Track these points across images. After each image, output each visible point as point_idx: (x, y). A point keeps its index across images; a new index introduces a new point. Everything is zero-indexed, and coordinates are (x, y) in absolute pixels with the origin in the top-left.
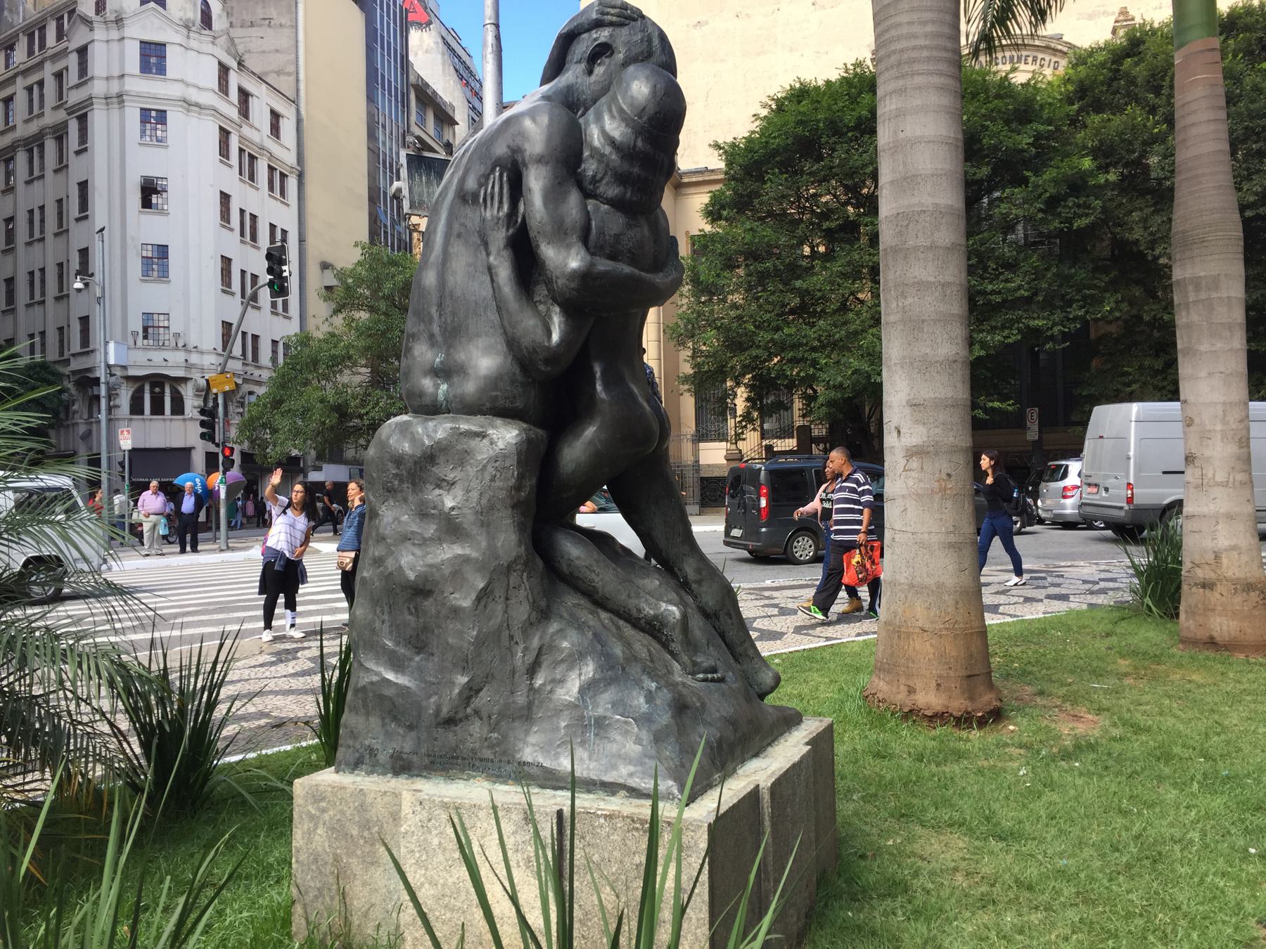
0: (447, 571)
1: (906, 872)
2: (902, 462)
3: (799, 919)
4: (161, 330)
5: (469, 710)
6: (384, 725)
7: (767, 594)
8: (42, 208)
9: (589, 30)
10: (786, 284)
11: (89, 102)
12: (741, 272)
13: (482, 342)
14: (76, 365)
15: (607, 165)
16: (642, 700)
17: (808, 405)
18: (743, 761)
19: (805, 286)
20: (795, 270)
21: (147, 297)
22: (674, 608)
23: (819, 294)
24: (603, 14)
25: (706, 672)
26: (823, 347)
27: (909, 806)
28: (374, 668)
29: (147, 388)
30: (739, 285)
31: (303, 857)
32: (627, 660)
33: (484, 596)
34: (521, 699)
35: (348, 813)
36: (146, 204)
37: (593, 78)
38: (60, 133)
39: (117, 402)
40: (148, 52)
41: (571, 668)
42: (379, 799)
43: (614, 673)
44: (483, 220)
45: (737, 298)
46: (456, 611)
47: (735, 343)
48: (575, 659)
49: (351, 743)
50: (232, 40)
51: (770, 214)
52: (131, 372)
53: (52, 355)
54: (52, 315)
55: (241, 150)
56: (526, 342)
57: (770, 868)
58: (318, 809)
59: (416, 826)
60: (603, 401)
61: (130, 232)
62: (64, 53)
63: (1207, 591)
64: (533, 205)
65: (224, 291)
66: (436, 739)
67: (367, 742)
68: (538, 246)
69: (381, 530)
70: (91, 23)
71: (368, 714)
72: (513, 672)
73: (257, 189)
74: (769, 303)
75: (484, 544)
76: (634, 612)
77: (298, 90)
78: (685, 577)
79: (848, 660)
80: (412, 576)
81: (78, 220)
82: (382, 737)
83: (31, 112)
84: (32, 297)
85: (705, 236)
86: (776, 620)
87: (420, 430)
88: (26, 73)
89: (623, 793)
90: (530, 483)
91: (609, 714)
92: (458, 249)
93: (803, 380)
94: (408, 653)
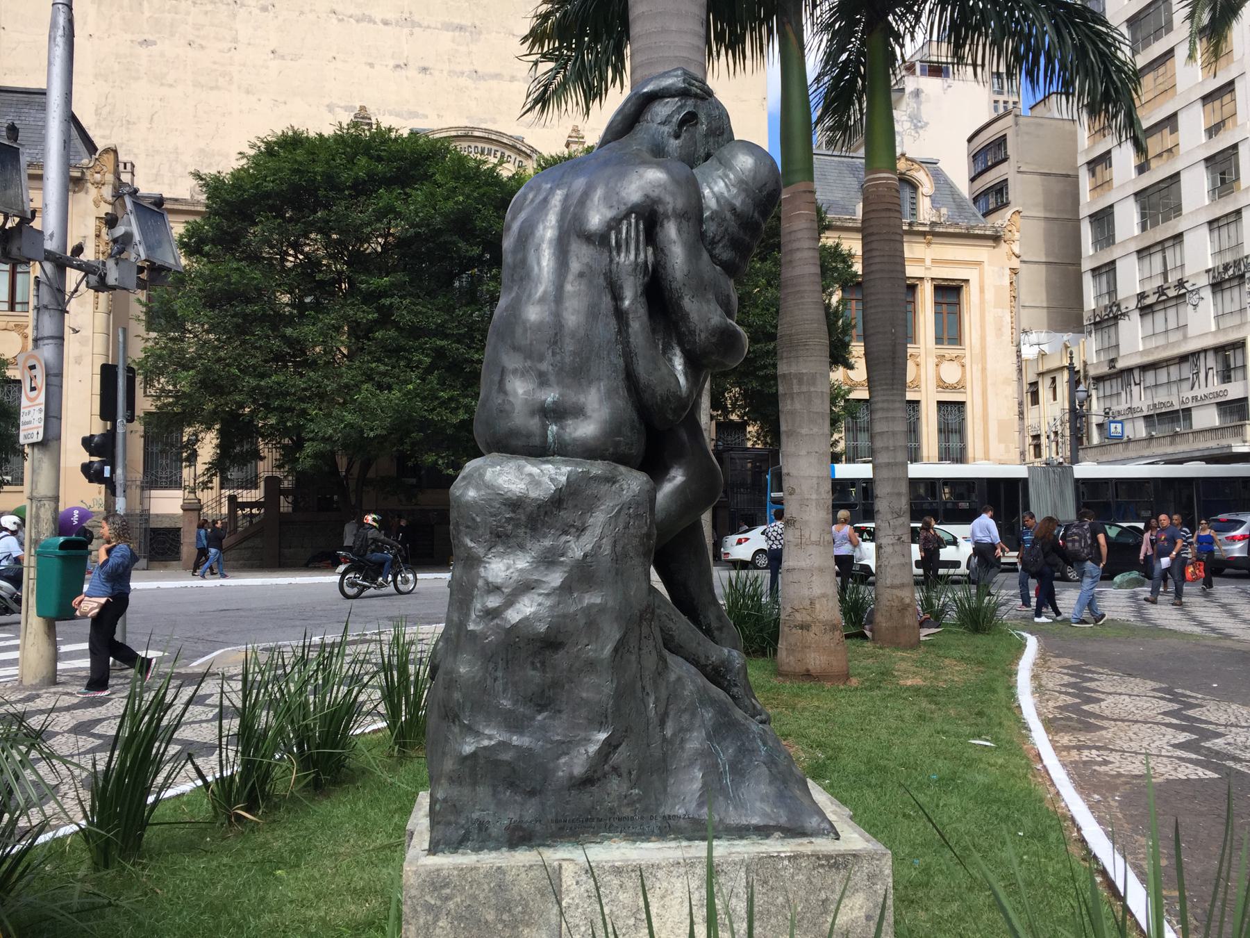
19: (295, 335)
42: (523, 875)
47: (210, 385)
49: (452, 818)
59: (581, 897)
66: (568, 803)
67: (475, 816)
72: (648, 724)
82: (492, 807)
89: (777, 834)
94: (528, 712)
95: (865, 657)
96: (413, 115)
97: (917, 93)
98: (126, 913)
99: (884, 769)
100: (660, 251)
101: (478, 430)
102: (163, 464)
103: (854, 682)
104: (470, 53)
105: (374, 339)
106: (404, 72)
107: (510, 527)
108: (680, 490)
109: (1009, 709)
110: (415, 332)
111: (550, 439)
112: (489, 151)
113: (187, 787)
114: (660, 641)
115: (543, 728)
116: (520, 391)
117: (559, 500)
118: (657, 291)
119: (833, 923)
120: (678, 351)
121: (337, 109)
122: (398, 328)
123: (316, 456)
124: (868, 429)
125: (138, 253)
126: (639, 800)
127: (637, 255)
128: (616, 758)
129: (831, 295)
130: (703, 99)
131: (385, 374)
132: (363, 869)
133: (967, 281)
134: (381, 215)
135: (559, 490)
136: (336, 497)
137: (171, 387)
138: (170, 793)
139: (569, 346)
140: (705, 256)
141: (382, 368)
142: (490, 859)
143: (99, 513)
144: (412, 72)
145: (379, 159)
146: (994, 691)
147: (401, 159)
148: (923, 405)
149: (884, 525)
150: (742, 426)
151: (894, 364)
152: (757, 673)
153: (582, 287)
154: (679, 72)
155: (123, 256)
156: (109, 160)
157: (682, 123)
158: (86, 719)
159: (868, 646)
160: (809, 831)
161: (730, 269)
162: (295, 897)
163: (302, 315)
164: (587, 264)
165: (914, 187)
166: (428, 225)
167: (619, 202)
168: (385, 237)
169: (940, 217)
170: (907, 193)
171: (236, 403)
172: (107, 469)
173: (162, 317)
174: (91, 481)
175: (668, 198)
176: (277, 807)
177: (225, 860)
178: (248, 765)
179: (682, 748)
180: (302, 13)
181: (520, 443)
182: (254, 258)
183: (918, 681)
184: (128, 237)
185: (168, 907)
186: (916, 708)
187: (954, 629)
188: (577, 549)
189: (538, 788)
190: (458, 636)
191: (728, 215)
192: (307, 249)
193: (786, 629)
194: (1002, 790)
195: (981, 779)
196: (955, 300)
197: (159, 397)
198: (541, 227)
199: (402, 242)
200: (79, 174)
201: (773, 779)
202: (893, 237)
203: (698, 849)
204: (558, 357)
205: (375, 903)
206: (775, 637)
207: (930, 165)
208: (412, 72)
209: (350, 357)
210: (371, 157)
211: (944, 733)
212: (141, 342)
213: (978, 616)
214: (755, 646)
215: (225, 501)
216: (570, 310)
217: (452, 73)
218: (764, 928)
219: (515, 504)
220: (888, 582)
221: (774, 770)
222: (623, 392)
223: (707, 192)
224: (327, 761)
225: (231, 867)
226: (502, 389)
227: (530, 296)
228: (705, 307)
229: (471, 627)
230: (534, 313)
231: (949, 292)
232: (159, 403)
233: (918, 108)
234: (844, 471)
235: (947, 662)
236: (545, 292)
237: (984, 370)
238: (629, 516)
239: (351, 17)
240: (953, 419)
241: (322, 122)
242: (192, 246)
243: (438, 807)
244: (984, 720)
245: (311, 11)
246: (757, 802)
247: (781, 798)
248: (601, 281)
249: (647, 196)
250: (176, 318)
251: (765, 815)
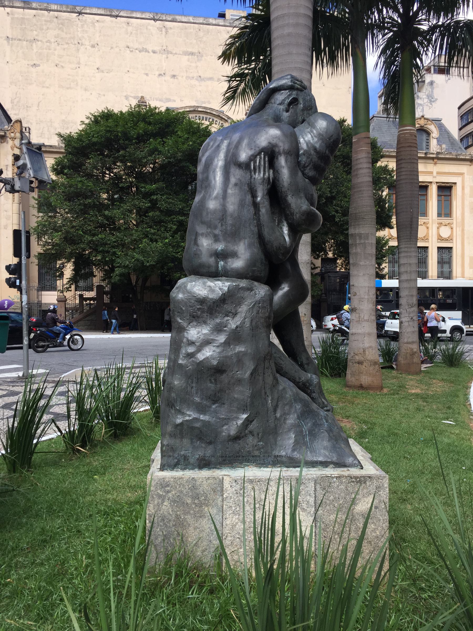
6: (192, 443)
42: (205, 482)
47: (69, 239)
49: (171, 454)
59: (233, 493)
63: (360, 365)
66: (227, 448)
67: (182, 453)
72: (268, 411)
82: (191, 449)
94: (208, 404)
95: (392, 379)
96: (168, 100)
97: (432, 83)
98: (22, 494)
99: (396, 434)
100: (276, 172)
101: (185, 264)
102: (48, 278)
103: (385, 390)
104: (197, 67)
105: (148, 216)
106: (163, 78)
107: (199, 313)
108: (286, 295)
109: (464, 405)
110: (169, 213)
111: (220, 268)
112: (203, 118)
113: (54, 435)
114: (274, 369)
115: (216, 412)
116: (205, 244)
117: (224, 299)
118: (275, 193)
120: (285, 224)
121: (130, 98)
122: (161, 211)
123: (121, 275)
124: (398, 262)
125: (30, 173)
126: (263, 448)
127: (264, 174)
128: (251, 427)
129: (382, 191)
130: (301, 91)
131: (154, 234)
132: (135, 476)
133: (455, 183)
134: (151, 152)
135: (224, 294)
136: (131, 296)
137: (50, 241)
138: (44, 439)
139: (230, 221)
140: (300, 174)
141: (152, 231)
142: (189, 474)
143: (18, 302)
144: (167, 78)
145: (150, 123)
146: (458, 396)
147: (161, 123)
148: (430, 249)
149: (404, 311)
150: (334, 261)
151: (411, 228)
152: (329, 385)
153: (237, 191)
154: (289, 77)
155: (22, 175)
156: (17, 126)
157: (290, 104)
158: (9, 401)
159: (394, 373)
160: (348, 464)
161: (314, 181)
162: (102, 489)
163: (113, 204)
164: (239, 179)
165: (428, 133)
166: (174, 158)
167: (255, 146)
168: (154, 164)
169: (442, 149)
170: (425, 136)
171: (82, 248)
172: (18, 281)
173: (45, 205)
174: (10, 287)
175: (281, 144)
176: (96, 446)
177: (70, 470)
178: (81, 426)
179: (285, 423)
180: (112, 48)
181: (204, 270)
182: (90, 176)
183: (418, 391)
184: (24, 165)
185: (43, 492)
186: (416, 404)
187: (440, 365)
188: (233, 324)
189: (213, 440)
190: (174, 366)
191: (312, 152)
192: (115, 171)
193: (351, 364)
194: (456, 446)
195: (446, 440)
196: (449, 194)
197: (44, 246)
198: (216, 160)
199: (162, 167)
200: (3, 134)
201: (330, 439)
202: (413, 161)
203: (294, 472)
204: (224, 227)
205: (140, 492)
206: (345, 367)
207: (437, 122)
208: (167, 78)
209: (137, 225)
210: (146, 122)
211: (429, 417)
212: (36, 218)
213: (452, 358)
214: (336, 372)
215: (77, 297)
216: (230, 203)
217: (188, 78)
218: (323, 511)
219: (202, 301)
220: (406, 340)
221: (331, 435)
222: (257, 245)
223: (302, 140)
224: (121, 425)
225: (73, 474)
226: (196, 243)
227: (210, 196)
228: (299, 200)
229: (180, 362)
230: (212, 205)
231: (446, 190)
232: (44, 248)
233: (432, 91)
234: (387, 283)
235: (434, 381)
236: (218, 194)
237: (463, 230)
238: (259, 307)
239: (136, 49)
240: (445, 256)
241: (121, 105)
242: (58, 170)
243: (164, 448)
244: (451, 411)
245: (116, 47)
246: (322, 449)
247: (334, 448)
248: (246, 188)
249: (270, 143)
250: (52, 206)
251: (325, 456)
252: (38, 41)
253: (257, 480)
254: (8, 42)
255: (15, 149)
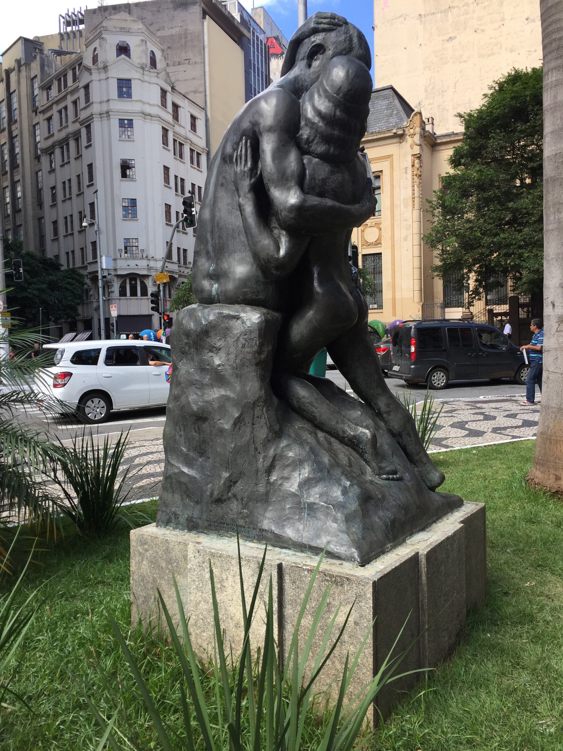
0: (216, 405)
1: (535, 607)
2: (555, 326)
3: (450, 638)
4: (134, 248)
5: (230, 494)
6: (182, 500)
7: (479, 405)
8: (70, 180)
9: (309, 36)
10: (503, 205)
11: (90, 118)
12: (473, 199)
13: (237, 256)
14: (90, 269)
15: (317, 130)
16: (339, 493)
17: (516, 283)
18: (411, 534)
19: (515, 206)
20: (510, 195)
21: (127, 229)
22: (367, 431)
23: (525, 211)
24: (318, 23)
25: (388, 473)
26: (527, 245)
27: (545, 559)
28: (176, 464)
29: (128, 281)
30: (471, 208)
31: (136, 577)
32: (332, 466)
33: (238, 422)
34: (261, 489)
35: (160, 553)
36: (124, 175)
37: (312, 70)
38: (76, 136)
39: (113, 289)
40: (121, 85)
41: (294, 470)
42: (176, 547)
43: (323, 474)
44: (236, 173)
45: (470, 216)
46: (221, 431)
47: (468, 245)
48: (297, 464)
49: (164, 509)
50: (168, 74)
51: (494, 160)
52: (120, 272)
53: (78, 264)
54: (77, 242)
55: (175, 141)
56: (263, 255)
57: (425, 607)
58: (143, 549)
59: (196, 565)
60: (318, 293)
61: (116, 192)
62: (76, 90)
64: (265, 161)
65: (167, 224)
66: (211, 511)
67: (173, 510)
68: (269, 190)
69: (179, 378)
70: (90, 70)
71: (173, 492)
72: (257, 471)
73: (184, 163)
74: (491, 218)
75: (238, 388)
76: (341, 433)
77: (206, 102)
78: (379, 409)
79: (523, 453)
80: (195, 408)
81: (88, 186)
83: (61, 125)
84: (67, 231)
85: (450, 176)
86: (481, 423)
87: (200, 314)
88: (57, 102)
90: (267, 349)
91: (317, 501)
92: (222, 193)
93: (512, 267)
119: (334, 620)
126: (248, 517)
128: (234, 490)
218: (294, 611)
252: (454, 8)
253: (218, 555)
254: (421, 21)
255: (415, 146)
